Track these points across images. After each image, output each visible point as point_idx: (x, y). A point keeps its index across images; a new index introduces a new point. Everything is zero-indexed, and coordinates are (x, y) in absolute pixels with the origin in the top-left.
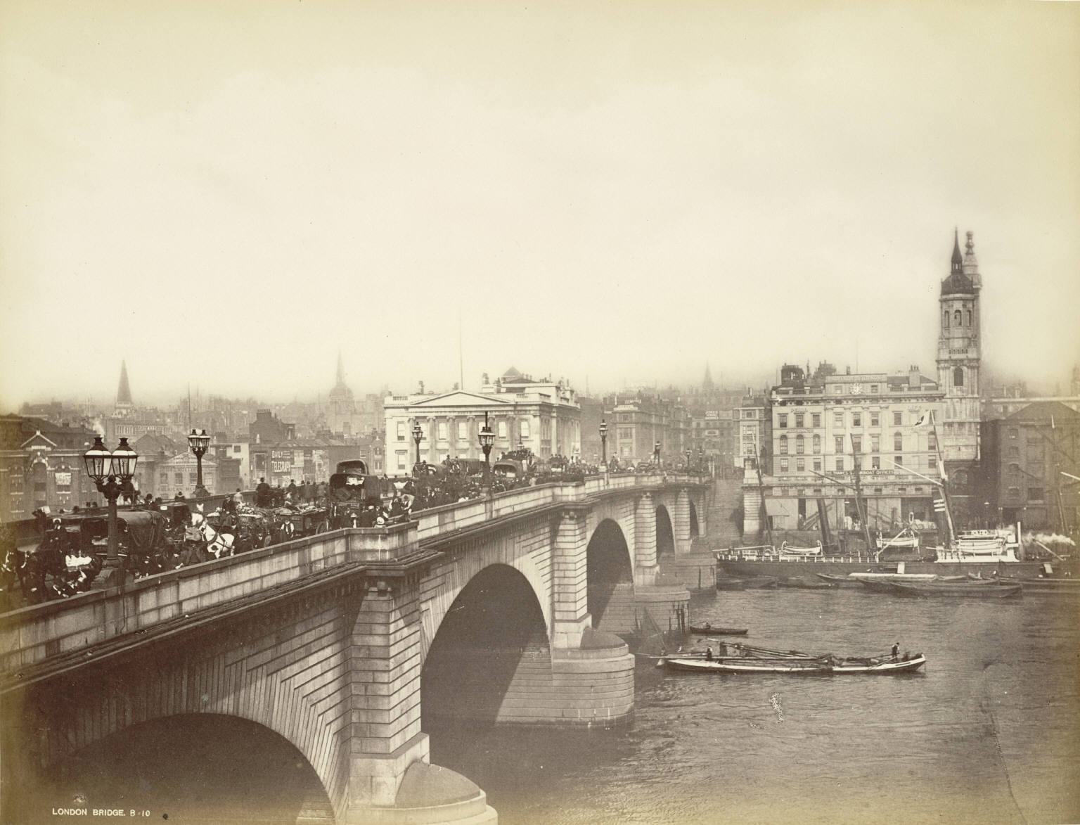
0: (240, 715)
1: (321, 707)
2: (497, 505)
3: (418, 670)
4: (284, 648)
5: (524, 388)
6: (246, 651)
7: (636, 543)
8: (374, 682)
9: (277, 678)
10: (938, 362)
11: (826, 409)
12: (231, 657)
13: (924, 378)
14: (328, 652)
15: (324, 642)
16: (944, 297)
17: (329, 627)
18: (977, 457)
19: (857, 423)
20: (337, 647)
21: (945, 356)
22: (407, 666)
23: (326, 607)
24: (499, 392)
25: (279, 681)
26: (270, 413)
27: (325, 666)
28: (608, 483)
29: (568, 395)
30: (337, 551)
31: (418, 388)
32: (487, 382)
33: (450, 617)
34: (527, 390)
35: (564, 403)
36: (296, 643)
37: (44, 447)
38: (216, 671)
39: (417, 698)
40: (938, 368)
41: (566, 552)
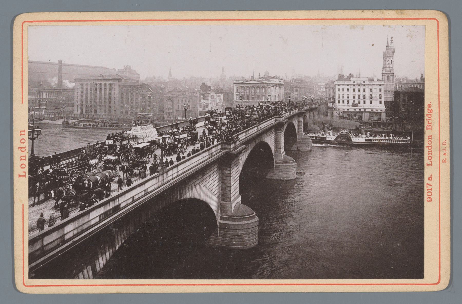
0: (193, 198)
1: (214, 191)
2: (260, 126)
3: (239, 178)
4: (204, 177)
5: (269, 79)
6: (194, 181)
7: (298, 127)
8: (227, 183)
9: (202, 186)
10: (382, 74)
11: (351, 87)
12: (192, 183)
13: (379, 79)
14: (215, 176)
15: (215, 173)
16: (385, 56)
17: (216, 169)
18: (393, 100)
19: (359, 91)
20: (218, 174)
21: (384, 72)
22: (236, 178)
23: (215, 164)
24: (263, 80)
25: (203, 186)
26: (205, 83)
27: (215, 180)
28: (290, 113)
29: (281, 81)
30: (218, 148)
31: (242, 78)
32: (260, 77)
33: (247, 160)
34: (270, 80)
35: (280, 83)
36: (207, 175)
37: (150, 92)
38: (186, 190)
39: (238, 185)
40: (382, 76)
41: (279, 135)
